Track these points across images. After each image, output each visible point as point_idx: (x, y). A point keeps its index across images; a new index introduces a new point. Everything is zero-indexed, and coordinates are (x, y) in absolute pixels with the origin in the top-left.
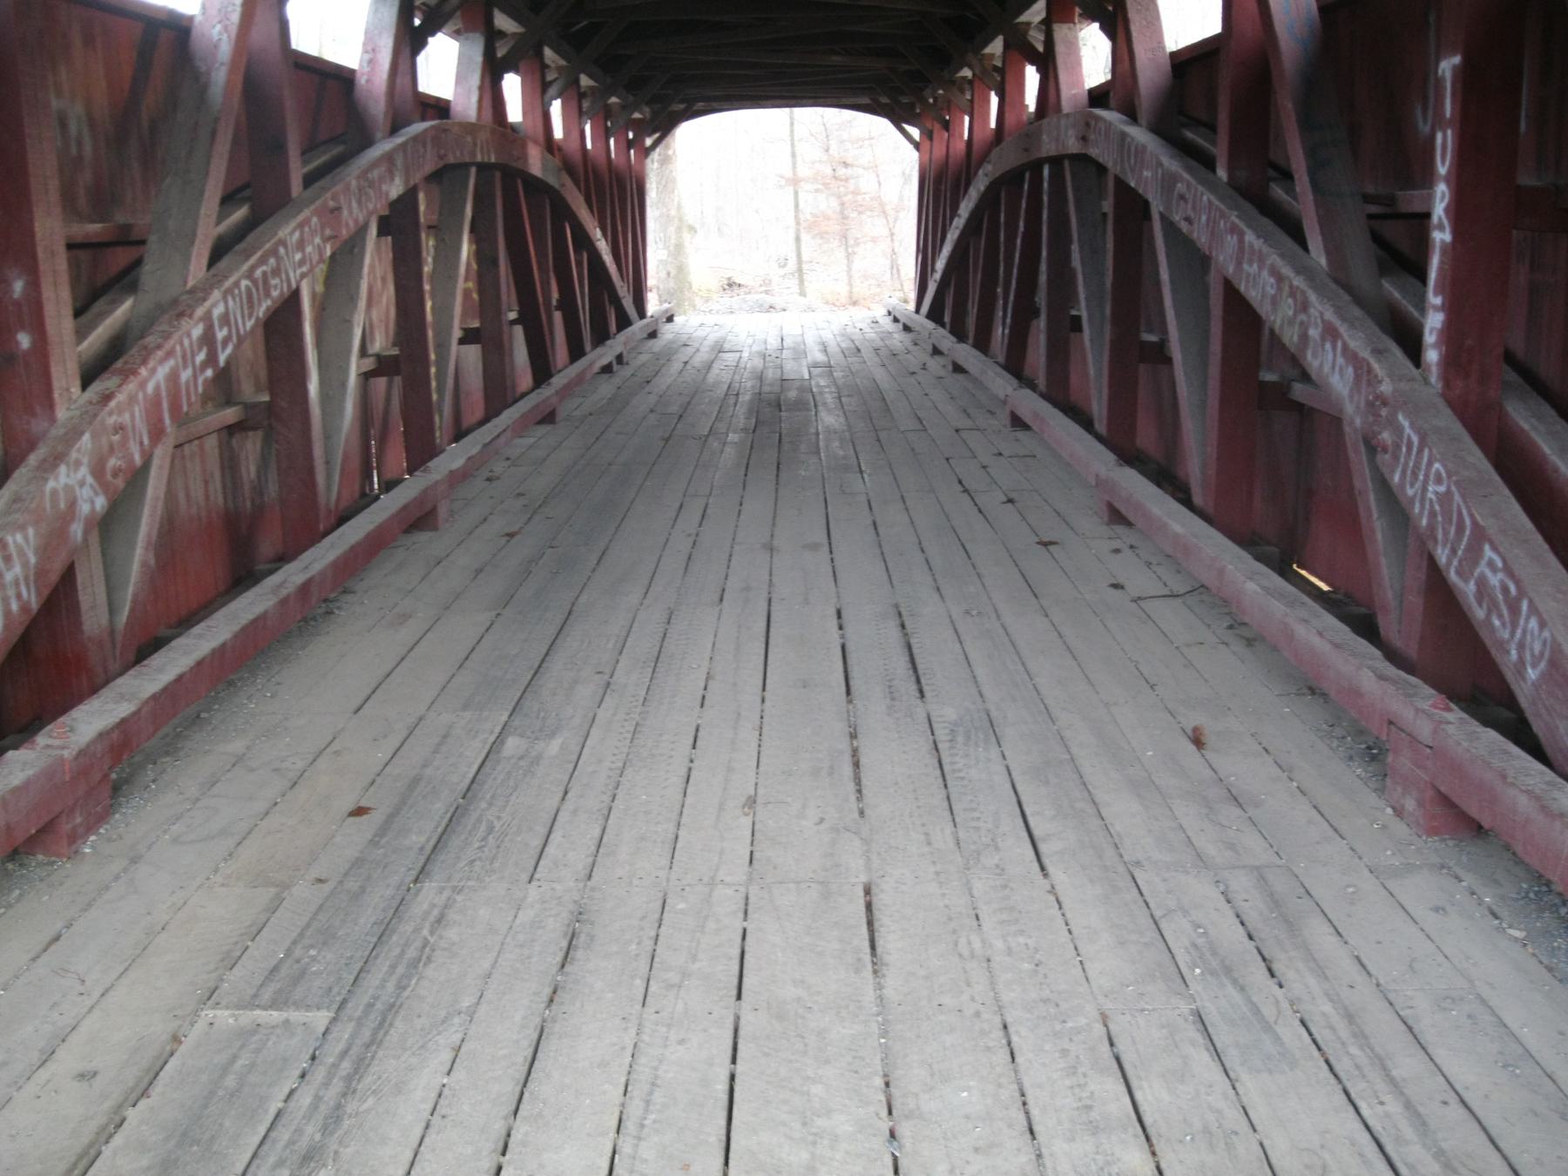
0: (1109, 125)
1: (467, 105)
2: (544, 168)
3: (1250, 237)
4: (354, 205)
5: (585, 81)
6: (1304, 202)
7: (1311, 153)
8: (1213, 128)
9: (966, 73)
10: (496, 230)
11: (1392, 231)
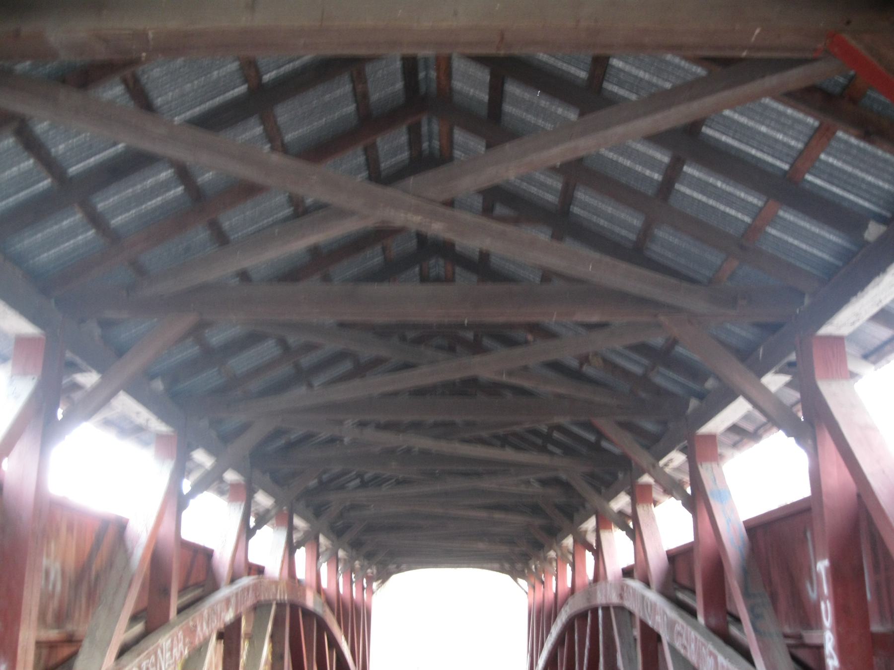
0: (634, 590)
1: (274, 567)
2: (315, 602)
3: (721, 659)
4: (205, 624)
5: (341, 553)
6: (747, 635)
7: (751, 610)
8: (693, 591)
9: (552, 554)
10: (284, 644)
11: (802, 654)
